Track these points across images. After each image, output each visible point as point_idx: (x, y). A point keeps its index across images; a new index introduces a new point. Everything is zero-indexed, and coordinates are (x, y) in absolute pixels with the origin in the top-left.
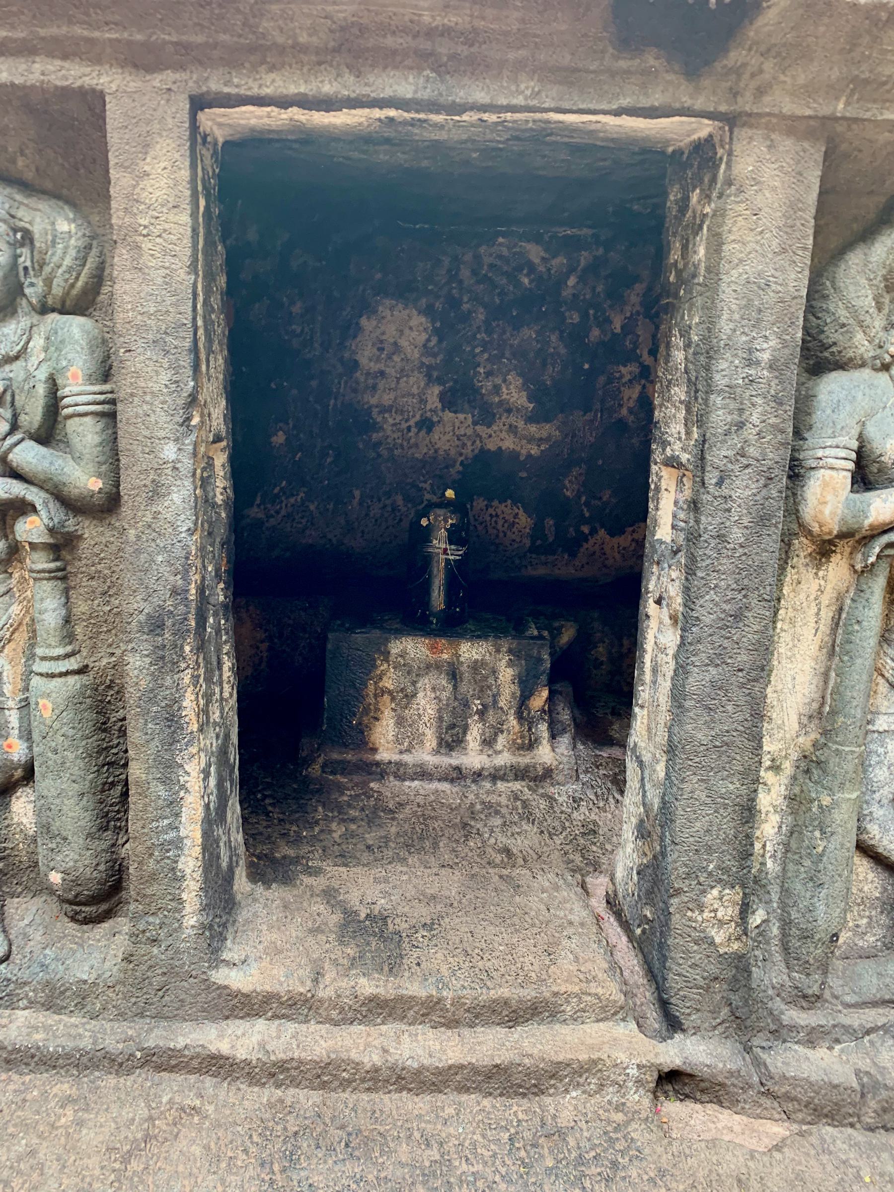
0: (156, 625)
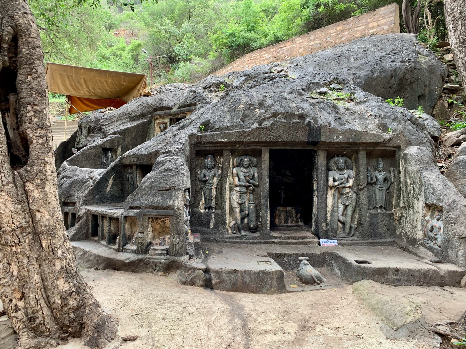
0: (265, 197)
